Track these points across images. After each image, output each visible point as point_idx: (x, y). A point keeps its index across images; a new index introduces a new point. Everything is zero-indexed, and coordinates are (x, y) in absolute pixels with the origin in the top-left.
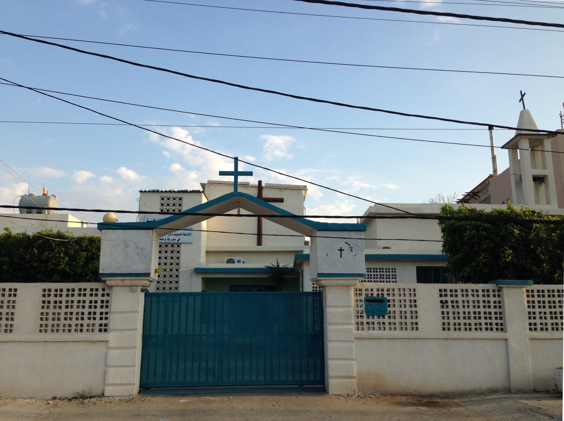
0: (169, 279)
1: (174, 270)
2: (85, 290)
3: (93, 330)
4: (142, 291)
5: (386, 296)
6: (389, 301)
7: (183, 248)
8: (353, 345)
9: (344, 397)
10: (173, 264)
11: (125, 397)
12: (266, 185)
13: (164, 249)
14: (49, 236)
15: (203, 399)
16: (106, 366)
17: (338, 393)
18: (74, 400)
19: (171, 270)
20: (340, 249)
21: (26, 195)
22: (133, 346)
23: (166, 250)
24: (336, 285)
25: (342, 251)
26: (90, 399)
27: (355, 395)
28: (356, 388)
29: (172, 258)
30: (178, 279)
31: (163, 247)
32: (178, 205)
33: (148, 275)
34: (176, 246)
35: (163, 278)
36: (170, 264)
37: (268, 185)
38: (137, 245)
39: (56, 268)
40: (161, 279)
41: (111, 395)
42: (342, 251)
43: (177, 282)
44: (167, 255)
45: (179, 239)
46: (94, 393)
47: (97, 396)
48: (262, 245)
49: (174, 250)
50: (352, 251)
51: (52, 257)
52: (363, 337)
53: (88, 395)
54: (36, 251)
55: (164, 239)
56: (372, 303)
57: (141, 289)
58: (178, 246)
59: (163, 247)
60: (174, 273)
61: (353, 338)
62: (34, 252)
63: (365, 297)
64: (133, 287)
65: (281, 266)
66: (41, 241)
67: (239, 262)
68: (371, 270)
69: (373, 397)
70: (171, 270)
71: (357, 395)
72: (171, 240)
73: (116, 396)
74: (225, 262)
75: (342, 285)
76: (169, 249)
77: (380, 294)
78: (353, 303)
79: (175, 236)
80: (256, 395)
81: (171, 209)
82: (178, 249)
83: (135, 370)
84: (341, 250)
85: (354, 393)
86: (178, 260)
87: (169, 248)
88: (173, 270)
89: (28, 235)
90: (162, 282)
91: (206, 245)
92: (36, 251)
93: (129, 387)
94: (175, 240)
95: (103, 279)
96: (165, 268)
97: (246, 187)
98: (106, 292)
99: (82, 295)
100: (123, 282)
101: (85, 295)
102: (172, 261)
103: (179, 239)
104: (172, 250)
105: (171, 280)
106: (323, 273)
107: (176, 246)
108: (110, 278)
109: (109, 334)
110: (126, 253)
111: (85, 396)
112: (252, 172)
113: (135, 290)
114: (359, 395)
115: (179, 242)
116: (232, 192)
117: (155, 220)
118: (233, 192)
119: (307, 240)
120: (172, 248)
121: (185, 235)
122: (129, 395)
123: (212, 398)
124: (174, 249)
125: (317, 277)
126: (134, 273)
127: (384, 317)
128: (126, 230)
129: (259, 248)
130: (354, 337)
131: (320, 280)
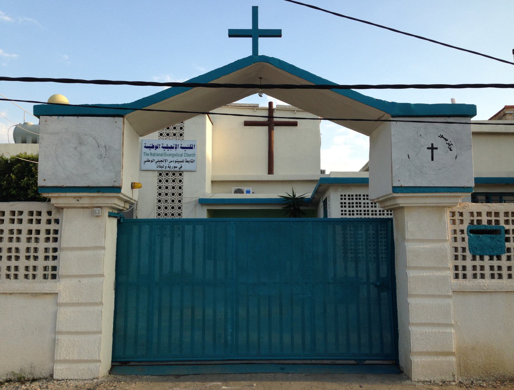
0: (171, 211)
1: (176, 201)
2: (21, 213)
3: (34, 276)
4: (110, 215)
5: (502, 223)
6: (507, 232)
7: (186, 177)
8: (450, 301)
9: (438, 385)
10: (175, 194)
11: (86, 382)
12: (278, 107)
13: (164, 178)
14: (29, 159)
15: (210, 386)
16: (56, 332)
17: (427, 379)
18: (6, 384)
19: (173, 201)
20: (431, 147)
21: (21, 124)
22: (97, 302)
23: (167, 179)
24: (421, 207)
25: (434, 150)
26: (31, 383)
27: (454, 381)
28: (455, 369)
29: (173, 188)
30: (181, 211)
31: (164, 176)
32: (179, 128)
33: (117, 189)
34: (177, 174)
35: (164, 209)
36: (171, 194)
37: (282, 107)
38: (99, 141)
39: (37, 196)
40: (162, 211)
41: (63, 378)
42: (434, 150)
43: (159, 201)
44: (169, 184)
45: (181, 166)
46: (37, 376)
47: (42, 379)
48: (273, 174)
49: (176, 179)
50: (451, 150)
51: (32, 183)
52: (467, 290)
53: (29, 376)
54: (13, 177)
55: (165, 167)
56: (481, 236)
57: (109, 213)
58: (180, 175)
59: (164, 176)
60: (176, 204)
61: (451, 290)
62: (12, 177)
63: (468, 226)
64: (95, 209)
65: (297, 196)
66: (19, 165)
67: (248, 192)
68: (351, 211)
69: (485, 385)
70: (173, 201)
71: (457, 382)
72: (171, 167)
73: (72, 380)
74: (233, 192)
75: (430, 207)
76: (170, 177)
77: (493, 221)
78: (449, 236)
79: (177, 163)
80: (294, 380)
81: (171, 133)
82: (180, 178)
83: (100, 340)
84: (432, 148)
85: (453, 378)
86: (180, 190)
87: (170, 177)
88: (175, 201)
89: (5, 159)
90: (164, 215)
91: (211, 174)
92: (13, 177)
93: (92, 366)
94: (177, 167)
95: (45, 195)
96: (166, 199)
97: (255, 110)
98: (53, 217)
99: (16, 221)
100: (78, 200)
101: (20, 221)
102: (173, 191)
103: (181, 166)
104: (174, 179)
105: (173, 213)
106: (403, 186)
107: (177, 174)
108: (56, 195)
109: (58, 283)
110: (81, 154)
111: (24, 378)
112: (280, 31)
113: (99, 213)
114: (460, 382)
115: (181, 169)
116: (251, 56)
117: (154, 145)
118: (252, 55)
119: (322, 169)
120: (174, 176)
121: (188, 162)
122: (92, 378)
123: (224, 387)
124: (175, 178)
125: (391, 192)
126: (94, 186)
127: (499, 258)
128: (80, 117)
129: (270, 177)
130: (452, 289)
131: (394, 198)
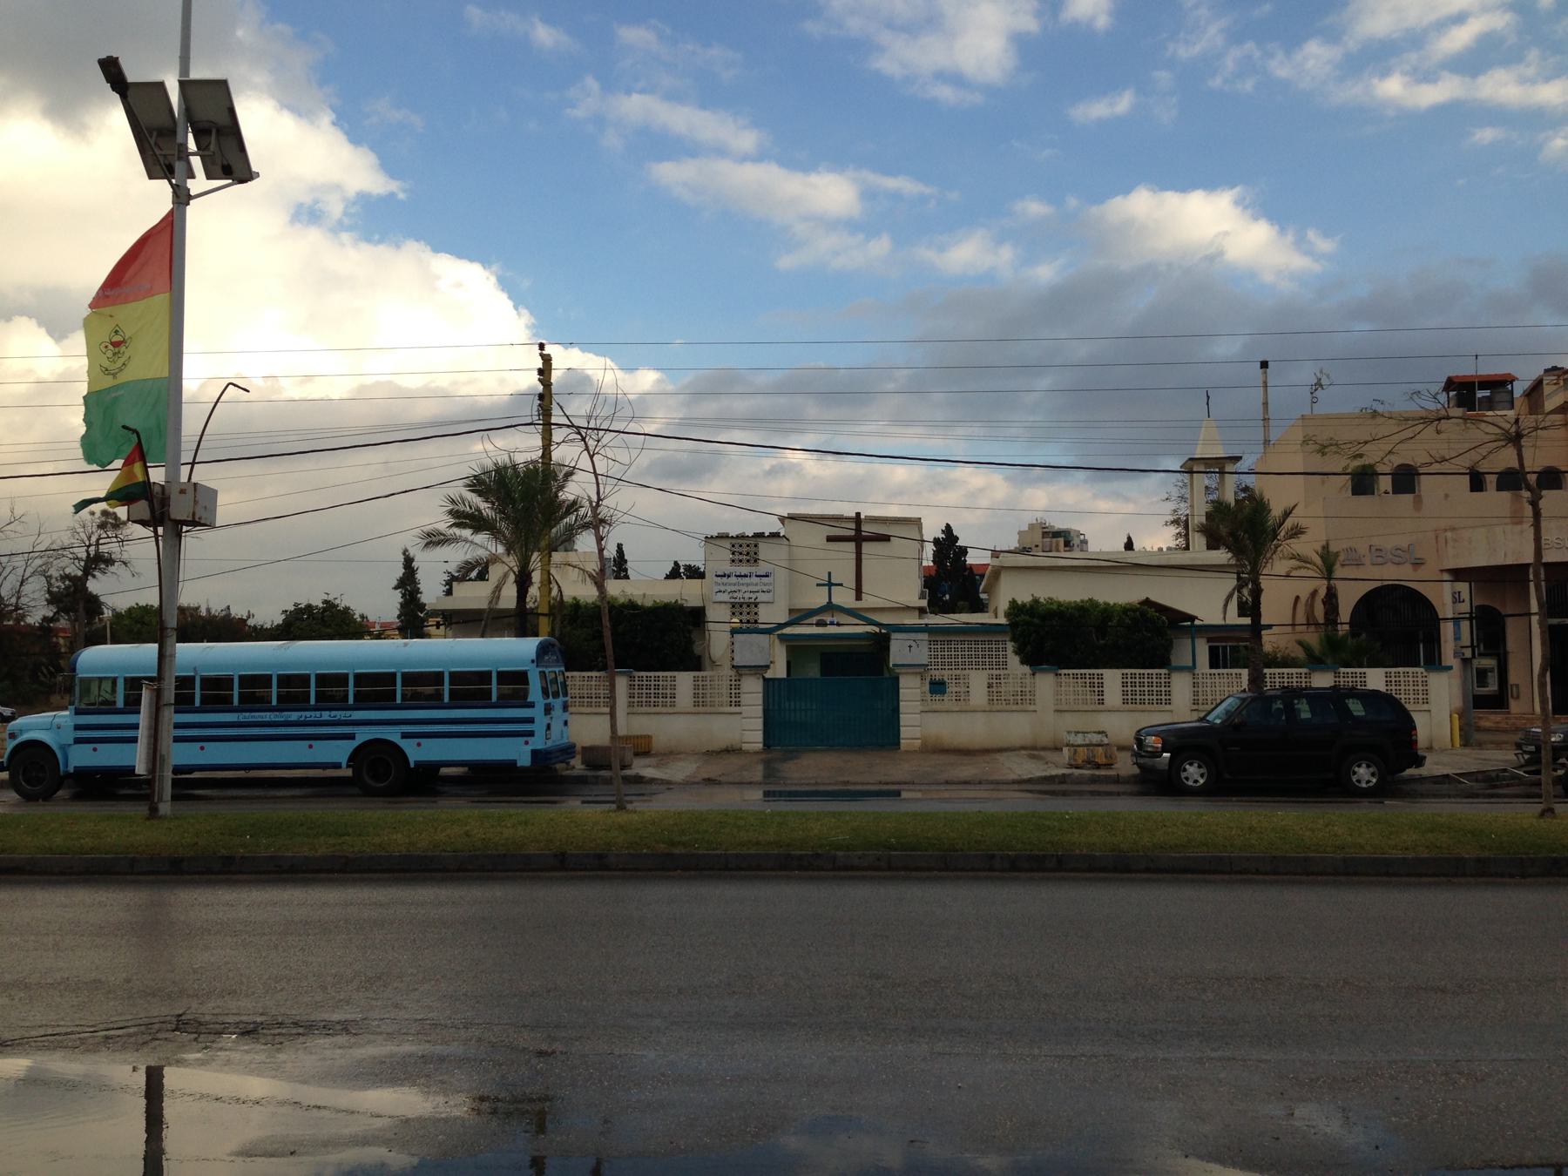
58: (756, 606)
82: (756, 610)
84: (910, 647)
87: (745, 610)
129: (859, 605)
